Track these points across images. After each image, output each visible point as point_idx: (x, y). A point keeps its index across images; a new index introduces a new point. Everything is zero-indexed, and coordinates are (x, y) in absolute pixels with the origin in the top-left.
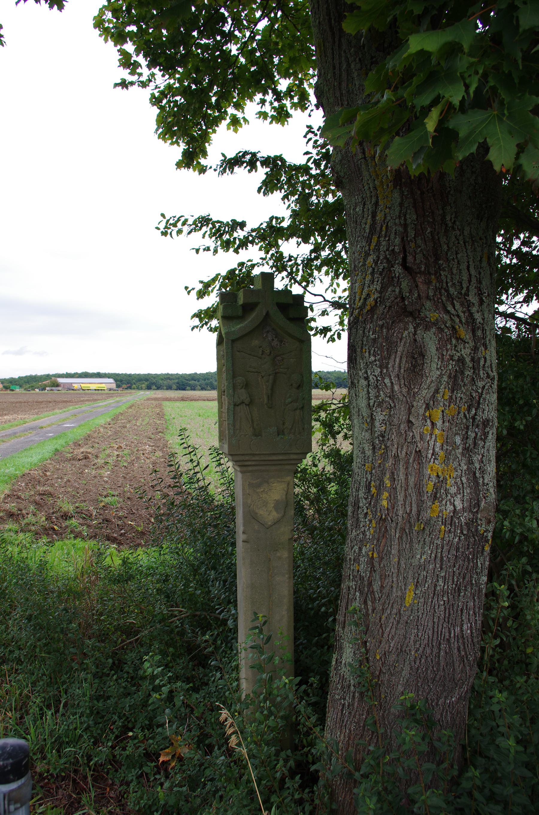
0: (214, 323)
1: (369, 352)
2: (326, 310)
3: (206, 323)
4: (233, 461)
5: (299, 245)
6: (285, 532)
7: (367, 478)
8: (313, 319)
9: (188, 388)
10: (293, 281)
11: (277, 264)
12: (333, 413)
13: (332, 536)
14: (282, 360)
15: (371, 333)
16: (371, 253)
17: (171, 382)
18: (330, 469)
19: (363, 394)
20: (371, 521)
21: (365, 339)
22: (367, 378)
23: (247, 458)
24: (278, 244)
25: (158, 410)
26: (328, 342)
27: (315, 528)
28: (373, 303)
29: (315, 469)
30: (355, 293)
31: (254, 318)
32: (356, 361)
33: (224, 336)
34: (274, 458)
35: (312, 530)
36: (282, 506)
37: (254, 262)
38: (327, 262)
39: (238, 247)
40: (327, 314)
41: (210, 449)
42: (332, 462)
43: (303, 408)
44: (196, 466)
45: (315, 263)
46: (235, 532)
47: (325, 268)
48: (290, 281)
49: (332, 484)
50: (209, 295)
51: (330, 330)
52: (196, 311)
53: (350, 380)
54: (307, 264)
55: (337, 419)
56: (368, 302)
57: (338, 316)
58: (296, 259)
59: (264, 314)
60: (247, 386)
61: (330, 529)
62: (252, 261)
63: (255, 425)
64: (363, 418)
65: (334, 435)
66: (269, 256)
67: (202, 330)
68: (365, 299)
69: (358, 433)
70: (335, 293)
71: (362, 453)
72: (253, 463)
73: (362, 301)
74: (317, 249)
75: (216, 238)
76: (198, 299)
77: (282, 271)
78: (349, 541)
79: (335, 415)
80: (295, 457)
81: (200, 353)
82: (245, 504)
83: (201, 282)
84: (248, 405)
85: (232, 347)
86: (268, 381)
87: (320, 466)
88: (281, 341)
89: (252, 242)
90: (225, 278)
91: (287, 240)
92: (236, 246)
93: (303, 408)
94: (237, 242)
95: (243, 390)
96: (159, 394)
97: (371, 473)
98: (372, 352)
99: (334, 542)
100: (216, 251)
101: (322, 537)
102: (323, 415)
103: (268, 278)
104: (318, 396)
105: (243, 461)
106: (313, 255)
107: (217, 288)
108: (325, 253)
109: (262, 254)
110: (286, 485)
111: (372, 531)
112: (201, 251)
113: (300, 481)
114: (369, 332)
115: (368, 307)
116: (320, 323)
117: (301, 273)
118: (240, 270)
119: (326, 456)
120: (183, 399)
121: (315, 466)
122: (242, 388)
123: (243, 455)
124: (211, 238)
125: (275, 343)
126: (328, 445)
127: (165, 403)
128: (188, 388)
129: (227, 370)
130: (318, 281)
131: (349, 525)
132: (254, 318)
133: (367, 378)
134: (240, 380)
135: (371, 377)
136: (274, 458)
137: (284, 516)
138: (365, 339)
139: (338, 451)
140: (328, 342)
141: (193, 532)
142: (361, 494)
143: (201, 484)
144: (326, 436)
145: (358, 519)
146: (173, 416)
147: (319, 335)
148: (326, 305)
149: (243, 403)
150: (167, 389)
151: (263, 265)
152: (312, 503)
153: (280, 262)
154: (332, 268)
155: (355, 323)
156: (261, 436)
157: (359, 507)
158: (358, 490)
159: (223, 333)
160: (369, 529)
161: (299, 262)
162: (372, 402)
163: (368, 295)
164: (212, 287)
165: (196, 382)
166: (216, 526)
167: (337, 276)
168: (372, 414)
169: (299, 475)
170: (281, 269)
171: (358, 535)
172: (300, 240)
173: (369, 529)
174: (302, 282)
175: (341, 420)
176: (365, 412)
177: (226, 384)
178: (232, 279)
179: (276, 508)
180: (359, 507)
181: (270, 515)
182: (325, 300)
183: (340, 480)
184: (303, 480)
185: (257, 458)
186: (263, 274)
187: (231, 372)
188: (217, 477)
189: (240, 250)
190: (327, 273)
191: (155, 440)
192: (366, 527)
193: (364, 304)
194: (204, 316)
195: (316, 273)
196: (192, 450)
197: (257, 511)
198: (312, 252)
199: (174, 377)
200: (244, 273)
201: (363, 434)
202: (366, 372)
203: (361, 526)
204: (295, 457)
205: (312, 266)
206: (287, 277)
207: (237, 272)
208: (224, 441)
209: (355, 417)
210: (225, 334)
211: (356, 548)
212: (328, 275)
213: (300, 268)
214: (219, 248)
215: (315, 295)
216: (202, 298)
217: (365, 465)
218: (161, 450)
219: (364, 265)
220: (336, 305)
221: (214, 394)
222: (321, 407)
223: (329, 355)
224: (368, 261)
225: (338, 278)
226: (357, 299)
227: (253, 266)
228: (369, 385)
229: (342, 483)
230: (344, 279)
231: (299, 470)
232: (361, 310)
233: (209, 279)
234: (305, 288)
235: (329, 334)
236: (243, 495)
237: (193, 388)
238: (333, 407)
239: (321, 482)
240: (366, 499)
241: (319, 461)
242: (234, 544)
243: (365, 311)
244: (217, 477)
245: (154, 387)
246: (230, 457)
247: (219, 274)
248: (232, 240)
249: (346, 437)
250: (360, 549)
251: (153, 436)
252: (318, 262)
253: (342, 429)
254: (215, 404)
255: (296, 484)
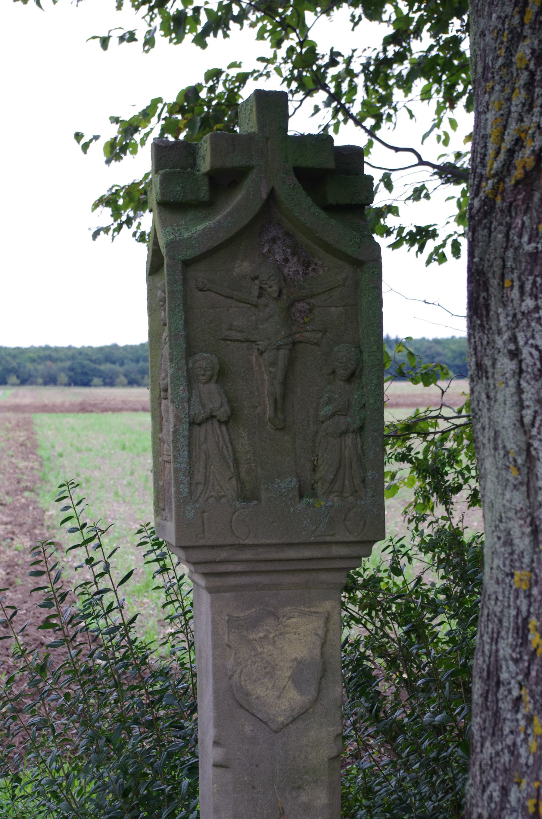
0: (147, 221)
1: (522, 287)
2: (423, 187)
3: (129, 222)
4: (188, 562)
5: (356, 24)
6: (319, 740)
7: (518, 609)
8: (392, 210)
9: (96, 380)
10: (341, 117)
11: (300, 73)
12: (444, 439)
13: (443, 747)
14: (310, 311)
15: (525, 238)
16: (527, 31)
17: (54, 367)
18: (434, 578)
19: (505, 393)
20: (529, 719)
21: (510, 254)
22: (515, 354)
23: (224, 554)
24: (304, 25)
25: (21, 436)
26: (428, 262)
27: (400, 728)
28: (531, 163)
29: (399, 580)
30: (485, 137)
31: (237, 205)
32: (488, 311)
33: (163, 251)
34: (291, 554)
35: (391, 733)
36: (314, 674)
37: (245, 69)
38: (425, 67)
39: (206, 32)
40: (427, 196)
41: (140, 532)
42: (440, 561)
43: (361, 428)
44: (101, 575)
45: (397, 69)
46: (196, 741)
47: (420, 83)
48: (334, 116)
49: (441, 618)
50: (134, 152)
51: (434, 235)
52: (104, 191)
53: (474, 359)
54: (377, 72)
55: (453, 455)
56: (518, 161)
57: (454, 202)
58: (348, 61)
59: (264, 196)
60: (221, 375)
61: (439, 729)
62: (239, 66)
63: (243, 474)
64: (507, 454)
65: (446, 494)
66: (282, 53)
67: (118, 237)
68: (511, 152)
69: (496, 494)
70: (446, 142)
71: (505, 544)
72: (240, 568)
73: (502, 156)
74: (401, 34)
75: (151, 9)
76: (108, 162)
77: (316, 90)
78: (475, 769)
79: (449, 445)
80: (343, 551)
81: (110, 297)
82: (220, 673)
83: (116, 120)
84: (226, 423)
85: (185, 281)
86: (274, 364)
87: (411, 572)
88: (307, 265)
89: (240, 19)
90: (174, 108)
91: (327, 11)
92: (200, 29)
93: (361, 428)
94: (204, 18)
95: (213, 386)
96: (26, 395)
97: (529, 596)
98: (528, 287)
99: (446, 764)
100: (150, 42)
101: (417, 750)
102: (418, 445)
103: (273, 106)
104: (401, 399)
105: (214, 562)
106: (392, 50)
107: (156, 133)
108: (421, 45)
109: (265, 48)
110: (321, 623)
111: (533, 745)
112: (113, 42)
113: (362, 608)
114: (520, 236)
115: (518, 174)
116: (411, 216)
117: (360, 95)
118: (212, 89)
119: (427, 547)
120: (83, 408)
121: (396, 570)
122: (209, 381)
123: (213, 547)
124: (137, 8)
125: (292, 267)
126: (430, 519)
127: (39, 418)
128: (96, 380)
129: (173, 337)
130: (402, 114)
131: (475, 729)
132: (237, 205)
133: (515, 354)
134: (203, 360)
135: (525, 352)
136: (291, 554)
137: (316, 700)
138: (510, 254)
139: (456, 533)
140: (428, 262)
141: (92, 739)
142: (505, 649)
143: (115, 617)
144: (427, 498)
145: (497, 714)
146: (59, 450)
147: (405, 246)
148: (424, 175)
149: (212, 417)
150: (45, 384)
151: (268, 75)
152: (392, 664)
153: (309, 70)
154: (438, 81)
155: (486, 214)
156: (258, 499)
157: (498, 683)
158: (495, 639)
159: (162, 243)
160: (525, 740)
161: (356, 67)
162: (528, 414)
163: (519, 142)
164: (143, 131)
165: (116, 367)
166: (151, 725)
167: (451, 100)
168: (529, 445)
169: (359, 594)
170: (311, 86)
171: (497, 754)
172: (359, 11)
173: (525, 740)
174: (363, 119)
175: (462, 457)
176: (512, 440)
177: (170, 371)
178: (192, 110)
179: (297, 679)
180: (498, 683)
181: (281, 698)
182: (422, 163)
183: (462, 604)
184: (370, 605)
185: (248, 555)
186: (259, 94)
187: (182, 341)
188: (152, 604)
189: (210, 39)
190: (426, 95)
191: (14, 509)
192: (518, 734)
193: (508, 165)
194: (121, 202)
195: (398, 94)
196: (92, 536)
197: (249, 687)
198: (388, 41)
199: (61, 355)
200: (220, 96)
201: (508, 496)
202: (514, 339)
203: (507, 730)
204: (343, 551)
205: (387, 77)
206: (327, 104)
207: (203, 94)
208: (166, 513)
209: (487, 452)
210: (167, 246)
211: (494, 789)
212: (429, 98)
213: (360, 81)
214: (158, 35)
215: (397, 150)
216: (118, 158)
217: (512, 575)
218: (30, 533)
219: (508, 64)
220: (448, 173)
221: (142, 394)
222: (411, 427)
223: (423, 298)
224: (518, 55)
225: (452, 107)
226: (491, 152)
227: (243, 78)
228: (521, 371)
229: (468, 616)
230: (468, 108)
231: (360, 580)
232: (501, 180)
233: (136, 111)
234: (371, 132)
235: (431, 245)
236: (215, 646)
237: (109, 381)
238: (443, 425)
239: (414, 609)
240: (516, 661)
241: (410, 559)
242: (193, 770)
243: (510, 182)
244: (152, 604)
245: (13, 379)
246: (182, 553)
247: (160, 100)
248: (190, 13)
249: (475, 499)
250: (505, 791)
251: (8, 500)
252: (404, 69)
253: (466, 481)
254: (147, 418)
255: (352, 617)
